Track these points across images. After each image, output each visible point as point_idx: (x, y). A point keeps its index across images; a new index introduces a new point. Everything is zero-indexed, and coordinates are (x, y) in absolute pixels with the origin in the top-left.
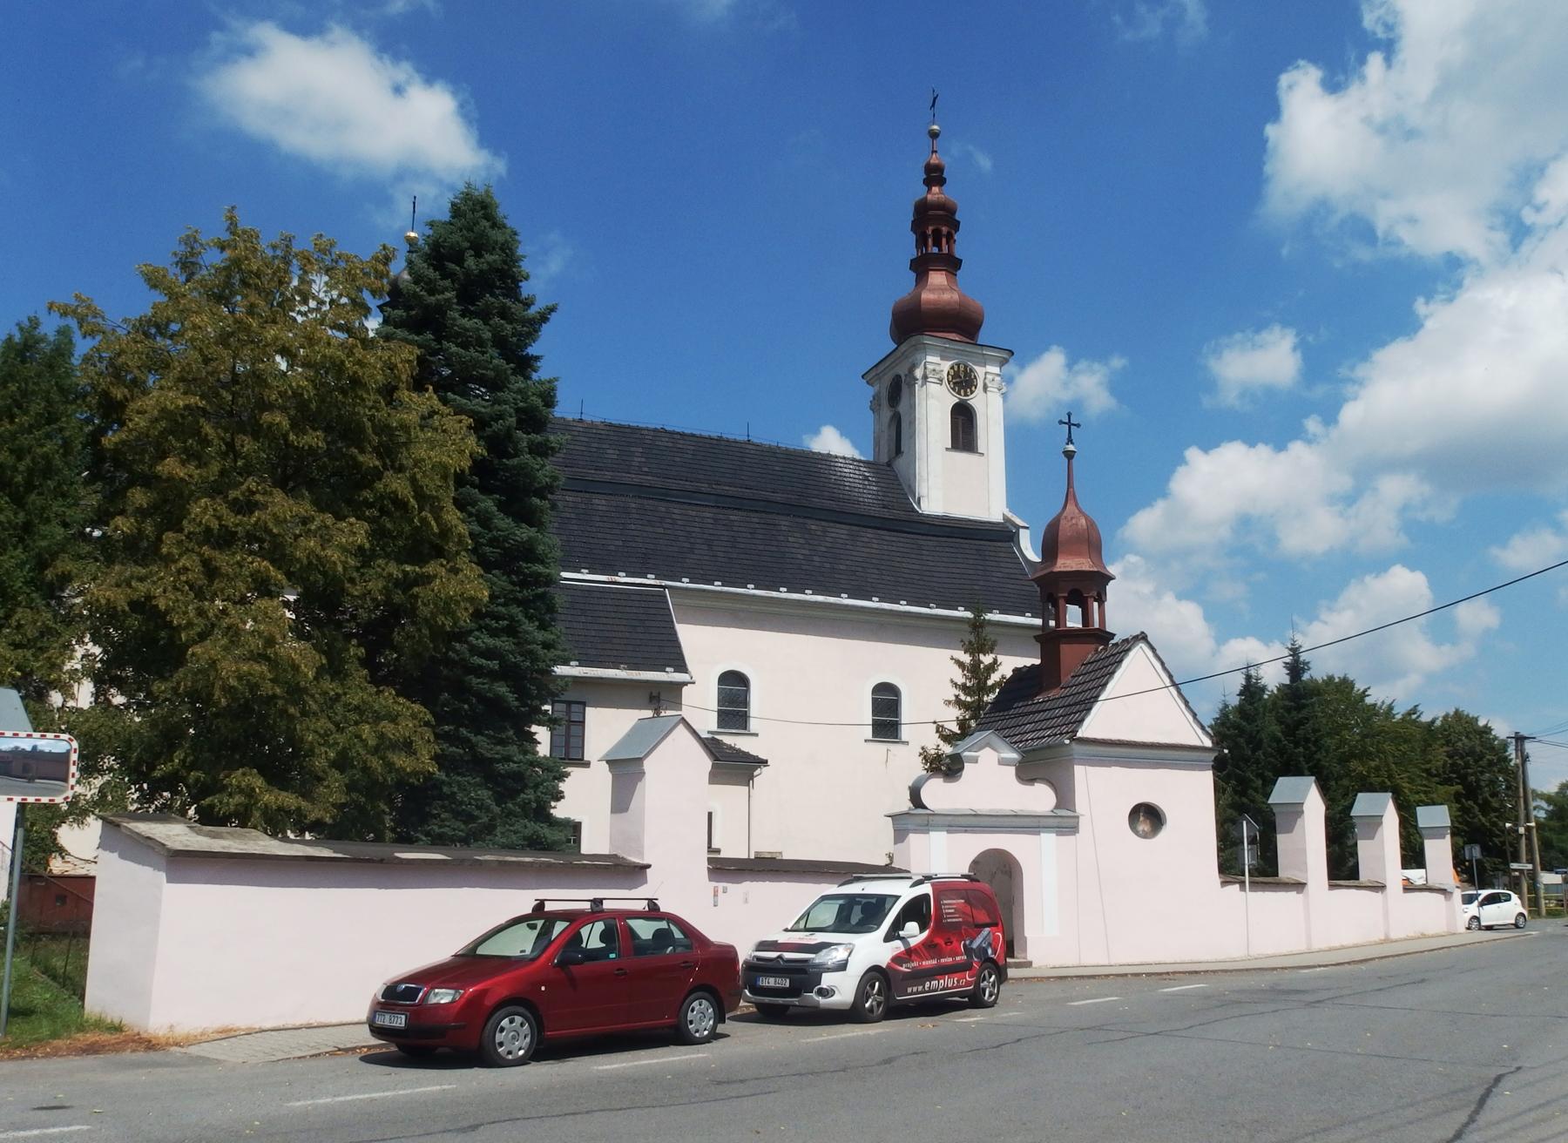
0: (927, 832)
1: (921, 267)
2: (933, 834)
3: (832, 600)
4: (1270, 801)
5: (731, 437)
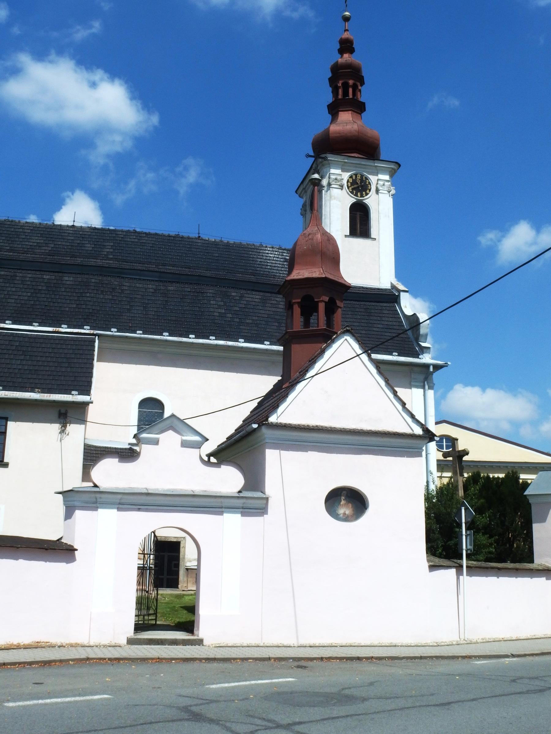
0: (96, 509)
1: (334, 110)
2: (100, 510)
3: (230, 343)
4: (525, 493)
5: (185, 235)
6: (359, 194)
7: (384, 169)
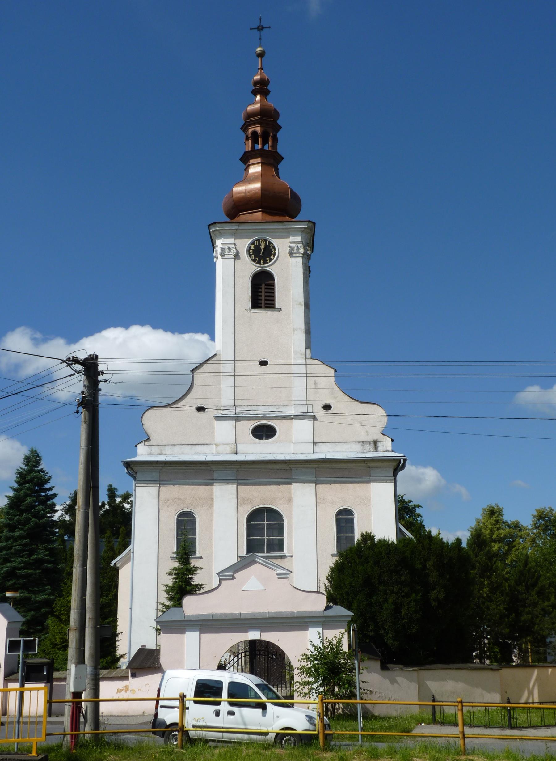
6: (262, 261)
7: (280, 230)
